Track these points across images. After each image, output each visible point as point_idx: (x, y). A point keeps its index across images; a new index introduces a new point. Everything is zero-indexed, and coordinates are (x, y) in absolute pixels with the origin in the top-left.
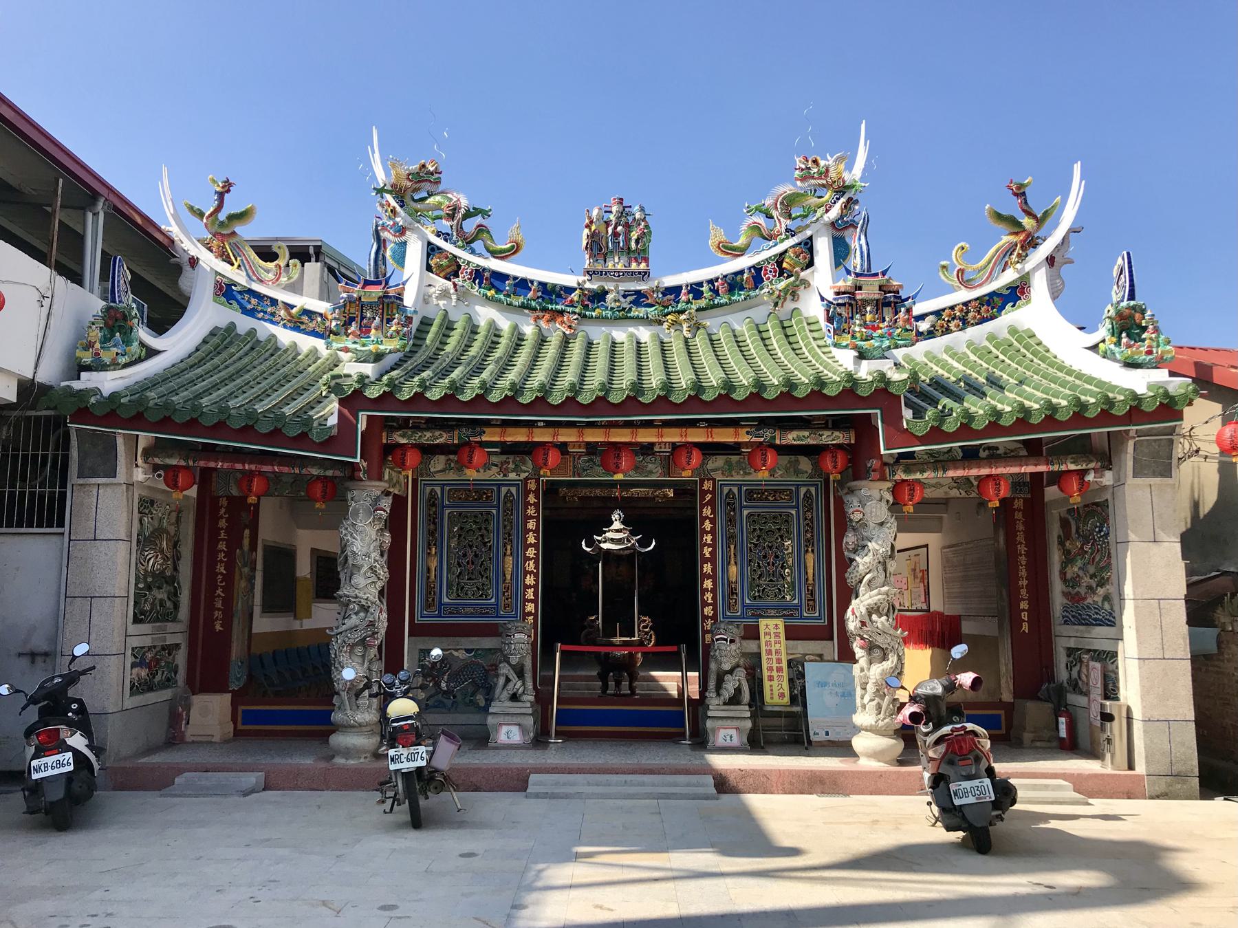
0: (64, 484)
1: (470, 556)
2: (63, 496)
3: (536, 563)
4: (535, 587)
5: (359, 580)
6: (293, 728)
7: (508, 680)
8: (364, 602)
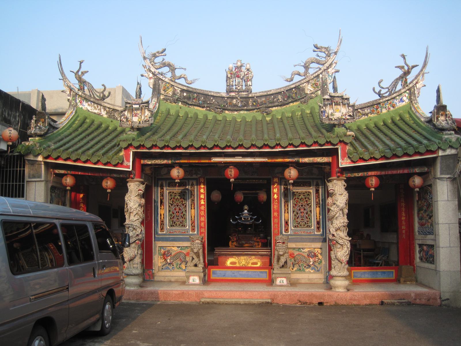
0: (23, 181)
1: (177, 210)
2: (23, 185)
3: (205, 212)
4: (204, 222)
5: (132, 217)
6: (153, 224)
7: (193, 259)
8: (135, 227)
